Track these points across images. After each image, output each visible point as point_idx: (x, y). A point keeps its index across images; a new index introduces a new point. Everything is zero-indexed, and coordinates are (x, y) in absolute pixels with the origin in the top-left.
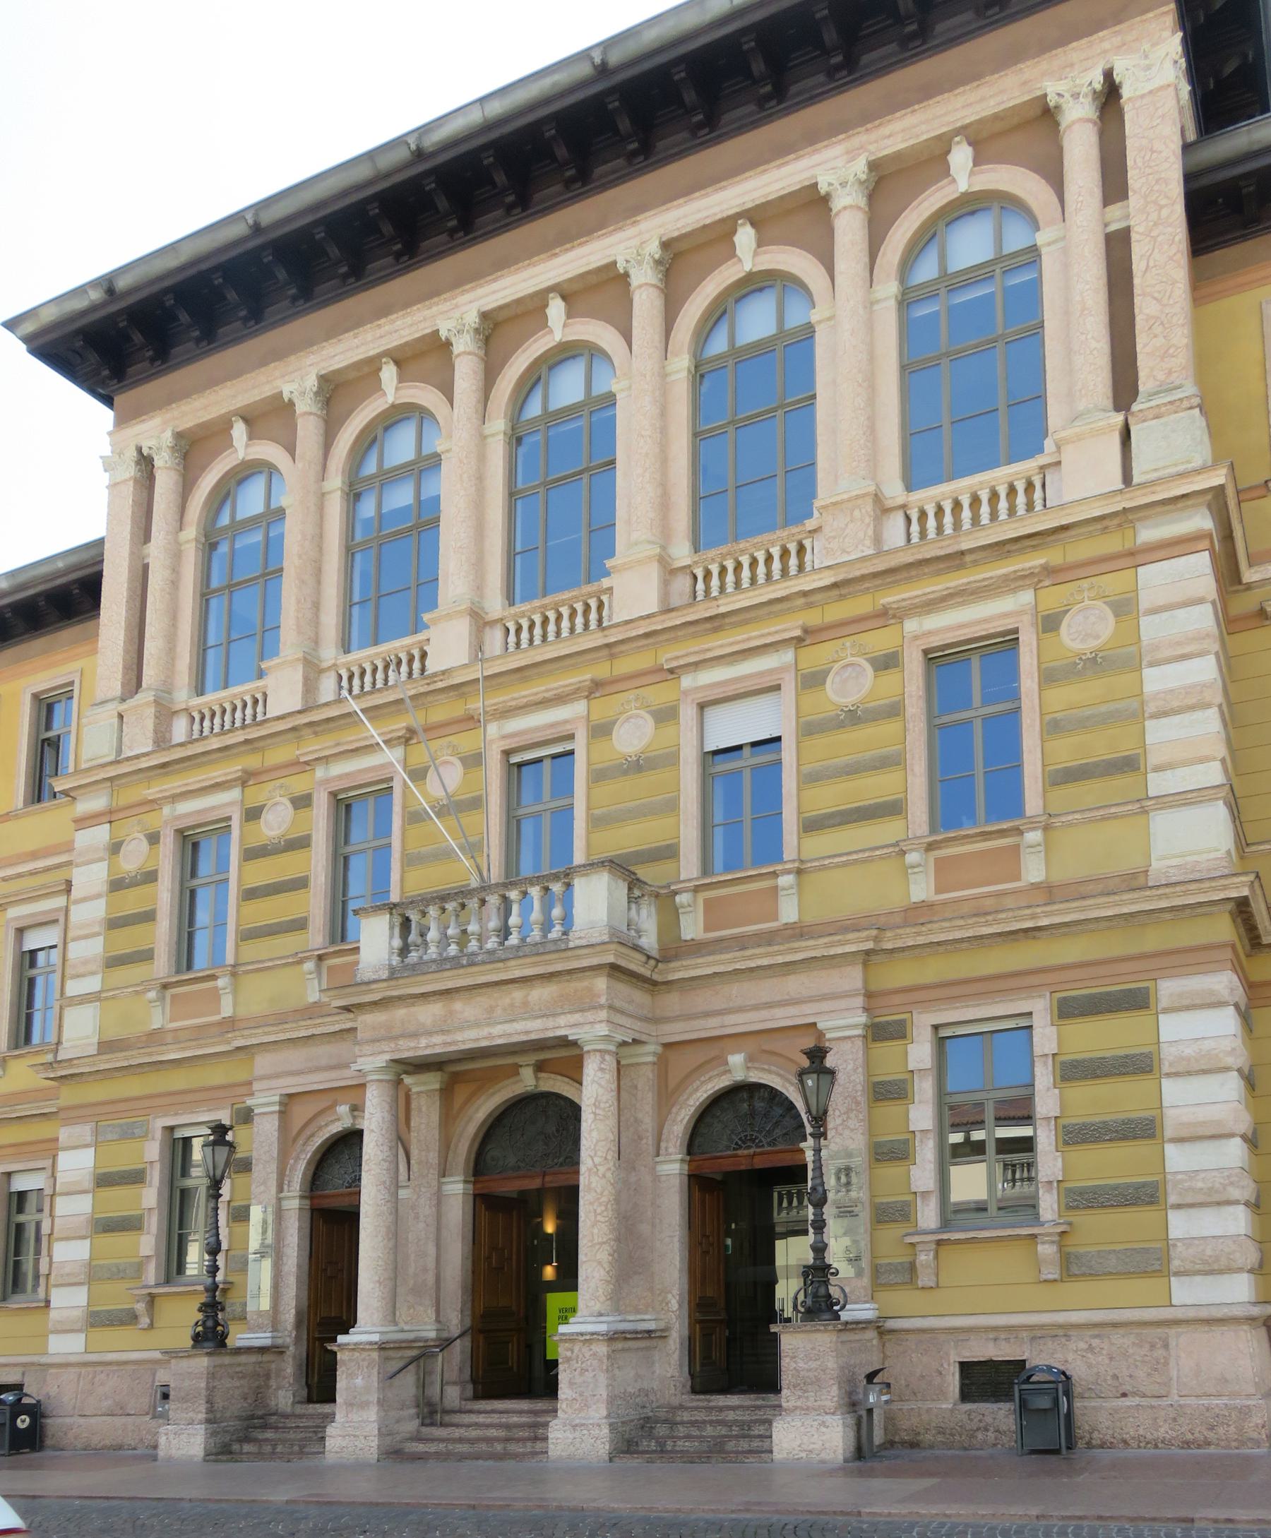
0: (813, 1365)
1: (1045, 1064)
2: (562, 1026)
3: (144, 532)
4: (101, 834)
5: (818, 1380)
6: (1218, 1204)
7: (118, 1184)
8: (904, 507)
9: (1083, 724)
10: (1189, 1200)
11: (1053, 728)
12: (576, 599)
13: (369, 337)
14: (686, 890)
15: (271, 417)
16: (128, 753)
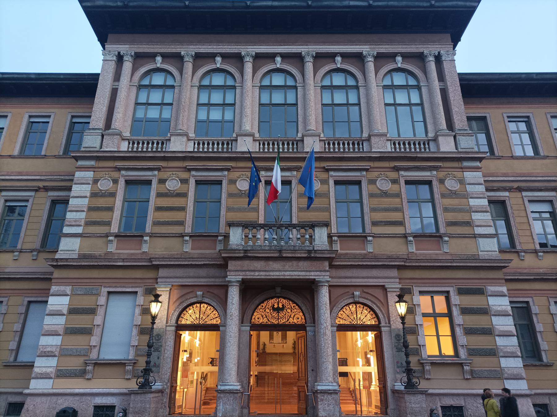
0: (417, 406)
1: (456, 307)
2: (312, 275)
3: (117, 77)
4: (90, 175)
5: (420, 411)
6: (514, 357)
7: (81, 313)
8: (194, 140)
9: (454, 210)
10: (506, 355)
11: (229, 209)
12: (216, 140)
13: (215, 47)
14: (336, 236)
15: (178, 58)
16: (104, 149)
